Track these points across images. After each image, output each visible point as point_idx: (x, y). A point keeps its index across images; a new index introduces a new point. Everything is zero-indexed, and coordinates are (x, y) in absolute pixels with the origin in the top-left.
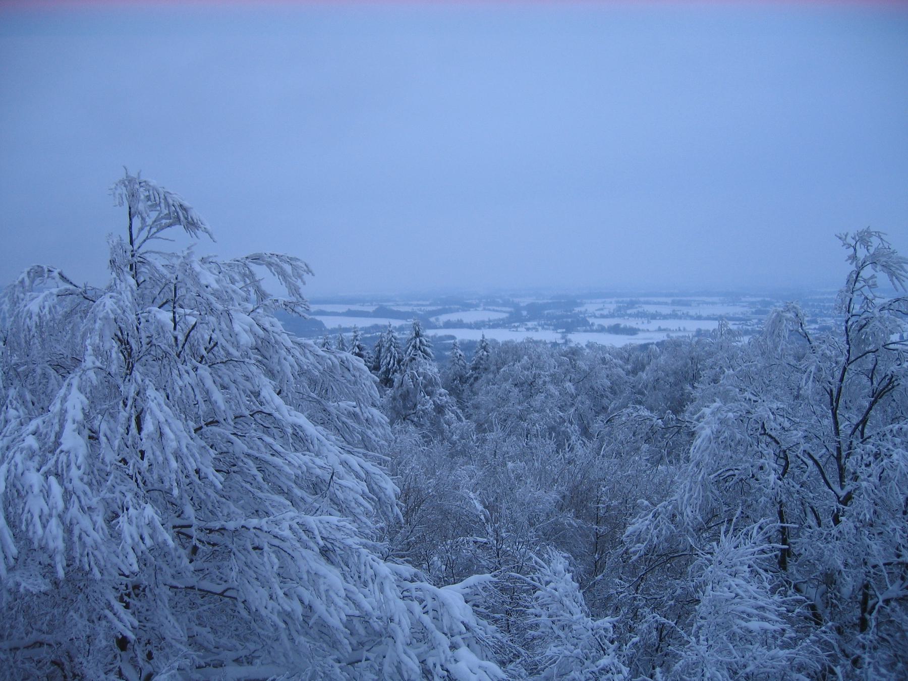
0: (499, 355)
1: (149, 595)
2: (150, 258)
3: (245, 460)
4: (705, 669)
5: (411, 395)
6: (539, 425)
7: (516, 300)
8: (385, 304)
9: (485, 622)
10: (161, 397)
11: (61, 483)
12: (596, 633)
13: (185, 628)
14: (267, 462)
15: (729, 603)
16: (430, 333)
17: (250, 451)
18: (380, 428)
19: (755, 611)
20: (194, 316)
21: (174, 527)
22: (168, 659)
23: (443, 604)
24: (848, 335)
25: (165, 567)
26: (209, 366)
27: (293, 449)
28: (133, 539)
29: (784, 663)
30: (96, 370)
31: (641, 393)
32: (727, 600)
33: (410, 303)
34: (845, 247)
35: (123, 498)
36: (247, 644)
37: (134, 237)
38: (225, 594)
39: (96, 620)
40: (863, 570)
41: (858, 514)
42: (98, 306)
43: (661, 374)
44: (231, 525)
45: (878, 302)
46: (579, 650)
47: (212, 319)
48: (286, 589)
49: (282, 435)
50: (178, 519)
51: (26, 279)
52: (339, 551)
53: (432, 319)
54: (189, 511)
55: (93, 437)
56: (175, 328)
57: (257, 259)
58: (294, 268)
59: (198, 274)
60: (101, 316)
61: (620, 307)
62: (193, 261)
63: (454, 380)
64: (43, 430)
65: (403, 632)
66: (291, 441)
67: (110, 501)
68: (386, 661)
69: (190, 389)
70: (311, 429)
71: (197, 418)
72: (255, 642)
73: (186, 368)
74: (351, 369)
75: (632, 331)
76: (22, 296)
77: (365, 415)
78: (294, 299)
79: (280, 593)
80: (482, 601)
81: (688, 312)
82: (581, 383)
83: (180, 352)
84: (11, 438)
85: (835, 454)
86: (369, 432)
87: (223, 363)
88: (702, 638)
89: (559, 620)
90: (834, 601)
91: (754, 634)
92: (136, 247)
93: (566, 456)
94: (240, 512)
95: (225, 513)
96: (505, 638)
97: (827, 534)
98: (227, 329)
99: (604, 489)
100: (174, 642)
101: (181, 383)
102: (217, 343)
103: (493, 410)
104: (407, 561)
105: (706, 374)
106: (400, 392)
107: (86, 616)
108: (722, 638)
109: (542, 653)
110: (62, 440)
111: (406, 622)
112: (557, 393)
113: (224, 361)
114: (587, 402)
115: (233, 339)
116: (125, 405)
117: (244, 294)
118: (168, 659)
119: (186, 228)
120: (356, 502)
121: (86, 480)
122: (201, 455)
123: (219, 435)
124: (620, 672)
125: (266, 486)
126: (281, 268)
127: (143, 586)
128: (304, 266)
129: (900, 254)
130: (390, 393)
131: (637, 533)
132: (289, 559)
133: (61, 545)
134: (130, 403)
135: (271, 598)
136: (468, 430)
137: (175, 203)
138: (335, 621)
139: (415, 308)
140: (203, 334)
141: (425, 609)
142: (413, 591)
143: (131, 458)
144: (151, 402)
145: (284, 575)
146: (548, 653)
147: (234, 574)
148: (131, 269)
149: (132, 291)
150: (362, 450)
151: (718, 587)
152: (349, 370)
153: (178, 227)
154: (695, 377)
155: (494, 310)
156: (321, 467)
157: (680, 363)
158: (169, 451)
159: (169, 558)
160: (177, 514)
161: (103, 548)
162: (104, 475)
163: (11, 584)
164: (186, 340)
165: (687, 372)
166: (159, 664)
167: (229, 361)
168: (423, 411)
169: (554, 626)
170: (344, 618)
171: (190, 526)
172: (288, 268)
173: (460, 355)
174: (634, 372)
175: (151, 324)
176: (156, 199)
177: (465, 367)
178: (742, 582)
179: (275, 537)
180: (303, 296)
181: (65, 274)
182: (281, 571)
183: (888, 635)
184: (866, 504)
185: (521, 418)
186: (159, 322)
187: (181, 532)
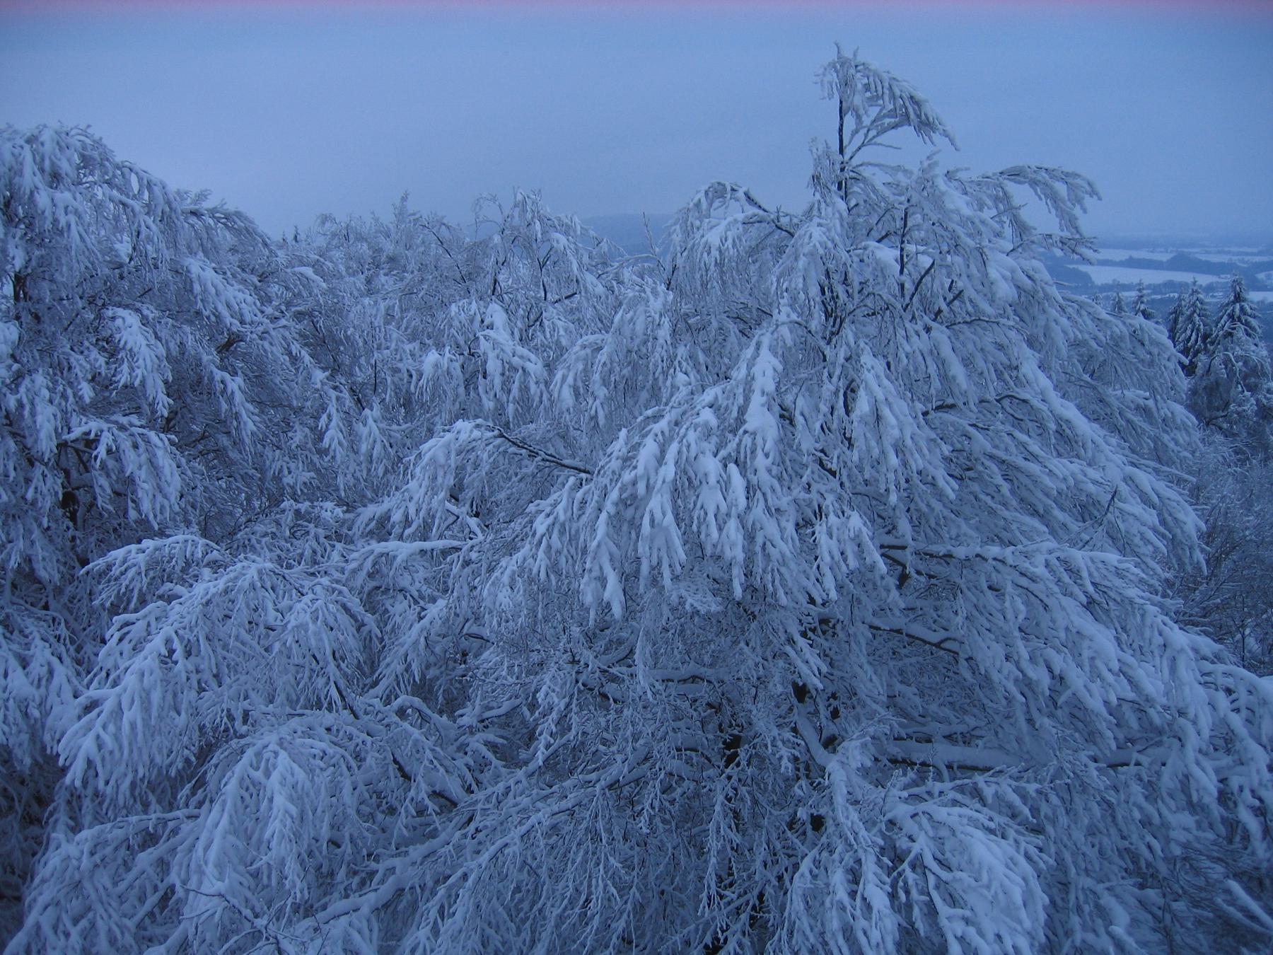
1: (841, 635)
2: (867, 172)
10: (880, 365)
11: (743, 474)
14: (1017, 468)
16: (1254, 296)
17: (995, 452)
18: (1184, 433)
20: (928, 254)
22: (859, 722)
27: (1055, 454)
28: (832, 558)
35: (821, 500)
37: (845, 143)
39: (770, 658)
42: (800, 237)
44: (961, 552)
49: (1040, 431)
51: (703, 200)
54: (904, 526)
55: (786, 417)
56: (902, 272)
57: (1015, 174)
59: (943, 194)
62: (936, 176)
64: (722, 401)
66: (1053, 441)
67: (802, 503)
69: (920, 358)
70: (1084, 427)
71: (928, 399)
73: (917, 327)
74: (1147, 343)
76: (697, 223)
77: (1162, 412)
78: (1066, 234)
84: (680, 410)
86: (1166, 438)
87: (966, 322)
92: (847, 157)
94: (973, 533)
95: (954, 533)
100: (869, 701)
101: (908, 348)
102: (961, 292)
104: (1207, 634)
110: (747, 417)
111: (1206, 721)
115: (986, 290)
116: (830, 376)
117: (997, 226)
118: (859, 721)
119: (918, 130)
121: (774, 472)
125: (1014, 503)
126: (1052, 188)
127: (833, 621)
132: (1041, 609)
133: (740, 555)
135: (1007, 658)
138: (1095, 704)
139: (1235, 258)
140: (939, 283)
141: (1235, 705)
142: (1220, 675)
147: (959, 619)
148: (840, 188)
150: (1152, 464)
152: (1143, 345)
153: (906, 128)
156: (1095, 482)
158: (888, 442)
161: (792, 565)
163: (674, 599)
170: (1114, 701)
171: (904, 548)
172: (1061, 189)
176: (879, 88)
179: (1022, 574)
181: (753, 194)
186: (877, 262)
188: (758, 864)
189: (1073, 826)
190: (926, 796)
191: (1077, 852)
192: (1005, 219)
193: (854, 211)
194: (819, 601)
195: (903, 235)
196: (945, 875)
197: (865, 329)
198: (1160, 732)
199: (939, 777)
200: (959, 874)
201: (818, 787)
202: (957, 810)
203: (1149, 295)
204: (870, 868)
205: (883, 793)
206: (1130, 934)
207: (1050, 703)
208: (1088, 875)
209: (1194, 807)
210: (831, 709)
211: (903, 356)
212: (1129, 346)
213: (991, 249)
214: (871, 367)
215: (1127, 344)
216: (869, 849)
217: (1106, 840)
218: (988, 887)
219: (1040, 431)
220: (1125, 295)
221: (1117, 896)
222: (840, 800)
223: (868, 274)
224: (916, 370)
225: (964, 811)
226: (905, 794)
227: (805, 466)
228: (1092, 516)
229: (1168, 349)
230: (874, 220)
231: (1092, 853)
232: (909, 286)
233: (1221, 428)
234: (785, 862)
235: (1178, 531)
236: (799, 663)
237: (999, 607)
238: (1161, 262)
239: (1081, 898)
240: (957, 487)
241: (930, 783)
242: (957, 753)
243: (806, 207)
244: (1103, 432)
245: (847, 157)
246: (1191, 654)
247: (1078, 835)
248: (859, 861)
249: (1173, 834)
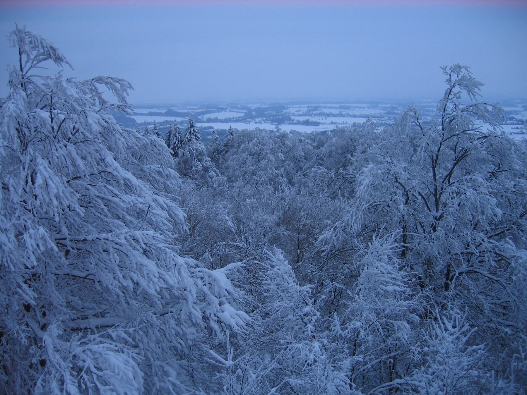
0: (239, 137)
1: (42, 280)
2: (34, 79)
3: (97, 199)
4: (362, 312)
7: (249, 106)
8: (171, 108)
9: (238, 289)
10: (45, 163)
12: (302, 294)
13: (65, 298)
14: (109, 200)
15: (376, 276)
16: (198, 125)
17: (99, 194)
18: (175, 180)
19: (391, 281)
21: (56, 240)
23: (215, 280)
24: (443, 125)
25: (51, 263)
26: (74, 144)
27: (124, 193)
29: (405, 308)
30: (4, 147)
31: (322, 159)
32: (375, 274)
33: (186, 107)
34: (445, 74)
35: (25, 223)
36: (101, 306)
37: (23, 66)
38: (87, 278)
39: (11, 295)
40: (449, 256)
41: (448, 226)
42: (4, 109)
43: (334, 148)
44: (90, 238)
45: (461, 107)
46: (292, 304)
47: (75, 116)
48: (123, 274)
49: (118, 184)
50: (57, 235)
52: (154, 251)
53: (200, 117)
54: (65, 230)
56: (52, 122)
57: (99, 80)
58: (122, 85)
59: (66, 88)
60: (8, 115)
61: (309, 109)
62: (62, 81)
63: (214, 153)
65: (192, 296)
66: (123, 188)
68: (183, 313)
69: (63, 158)
70: (135, 181)
71: (68, 175)
72: (105, 305)
73: (60, 145)
74: (157, 146)
75: (316, 124)
77: (166, 173)
78: (121, 104)
79: (121, 276)
80: (236, 277)
81: (348, 113)
83: (56, 136)
85: (434, 193)
86: (168, 183)
88: (361, 295)
89: (281, 287)
90: (432, 274)
91: (390, 293)
92: (24, 73)
94: (95, 230)
95: (86, 230)
96: (250, 298)
97: (430, 237)
98: (84, 122)
99: (302, 214)
100: (58, 306)
101: (57, 154)
102: (78, 129)
103: (237, 169)
104: (192, 257)
105: (359, 148)
107: (5, 292)
108: (372, 295)
109: (272, 306)
111: (194, 291)
112: (274, 160)
113: (83, 141)
114: (292, 164)
115: (88, 128)
116: (24, 168)
117: (92, 101)
118: (55, 316)
119: (55, 61)
120: (163, 223)
122: (71, 197)
123: (81, 185)
124: (315, 315)
125: (110, 215)
126: (114, 85)
127: (38, 275)
128: (128, 85)
129: (476, 80)
130: (177, 160)
131: (325, 240)
134: (27, 167)
135: (115, 279)
136: (222, 181)
137: (48, 46)
138: (152, 291)
139: (190, 111)
141: (204, 283)
143: (29, 199)
144: (40, 166)
145: (122, 266)
146: (275, 305)
147: (93, 266)
148: (22, 86)
149: (24, 99)
150: (164, 193)
151: (370, 267)
152: (156, 147)
153: (50, 60)
154: (353, 150)
155: (236, 112)
156: (142, 203)
157: (344, 142)
159: (53, 257)
160: (57, 232)
161: (15, 253)
162: (13, 210)
164: (59, 129)
165: (348, 147)
166: (50, 319)
167: (85, 140)
169: (278, 290)
170: (158, 289)
171: (65, 239)
172: (118, 86)
173: (217, 138)
174: (318, 147)
175: (37, 119)
176: (35, 43)
177: (220, 145)
178: (384, 264)
179: (116, 244)
180: (128, 102)
182: (120, 263)
183: (460, 292)
184: (452, 220)
185: (253, 174)
186: (41, 118)
187: (59, 242)
188: (18, 387)
189: (150, 342)
190: (88, 342)
191: (153, 352)
192: (96, 98)
193: (29, 96)
194: (30, 267)
195: (51, 106)
196: (100, 373)
197: (39, 147)
198: (178, 298)
199: (93, 333)
200: (105, 372)
201: (41, 348)
202: (102, 345)
204: (68, 377)
205: (69, 344)
206: (177, 379)
207: (135, 294)
208: (158, 360)
209: (195, 325)
210: (42, 312)
211: (55, 158)
212: (150, 147)
213: (89, 111)
214: (42, 164)
216: (67, 370)
217: (164, 345)
218: (118, 374)
219: (118, 184)
220: (149, 126)
221: (171, 366)
222: (50, 350)
223: (38, 123)
224: (62, 163)
225: (105, 345)
226: (79, 343)
227: (16, 209)
228: (142, 216)
229: (165, 148)
230: (39, 100)
231: (159, 351)
232: (56, 128)
233: (190, 177)
234: (30, 383)
235: (177, 218)
236: (24, 295)
237: (108, 258)
238: (162, 113)
239: (157, 370)
240: (84, 211)
241: (89, 336)
242: (100, 321)
243: (7, 95)
245: (24, 73)
246: (186, 266)
247: (152, 345)
248: (62, 376)
249: (188, 337)
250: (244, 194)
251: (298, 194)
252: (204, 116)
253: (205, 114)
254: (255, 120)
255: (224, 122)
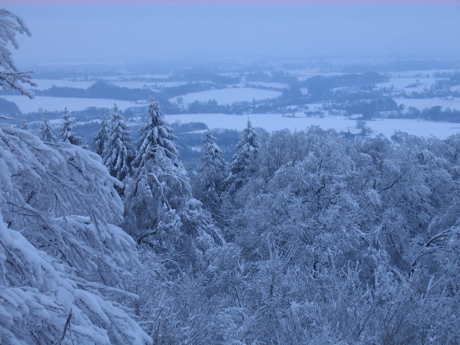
0: (271, 150)
5: (149, 208)
6: (332, 249)
7: (292, 73)
8: (104, 78)
18: (124, 253)
27: (7, 283)
33: (141, 76)
53: (173, 100)
61: (440, 82)
63: (208, 186)
66: (5, 271)
74: (84, 169)
77: (103, 235)
82: (389, 190)
86: (108, 259)
93: (376, 293)
99: (431, 339)
106: (133, 204)
112: (356, 205)
114: (400, 217)
139: (149, 85)
152: (80, 171)
155: (260, 87)
156: (50, 308)
168: (166, 230)
173: (216, 151)
177: (222, 168)
203: (74, 122)
212: (68, 173)
215: (66, 171)
220: (52, 122)
229: (103, 173)
233: (151, 245)
238: (81, 91)
244: (50, 258)
250: (285, 290)
251: (421, 291)
252: (183, 97)
253: (185, 94)
254: (307, 108)
255: (231, 113)
